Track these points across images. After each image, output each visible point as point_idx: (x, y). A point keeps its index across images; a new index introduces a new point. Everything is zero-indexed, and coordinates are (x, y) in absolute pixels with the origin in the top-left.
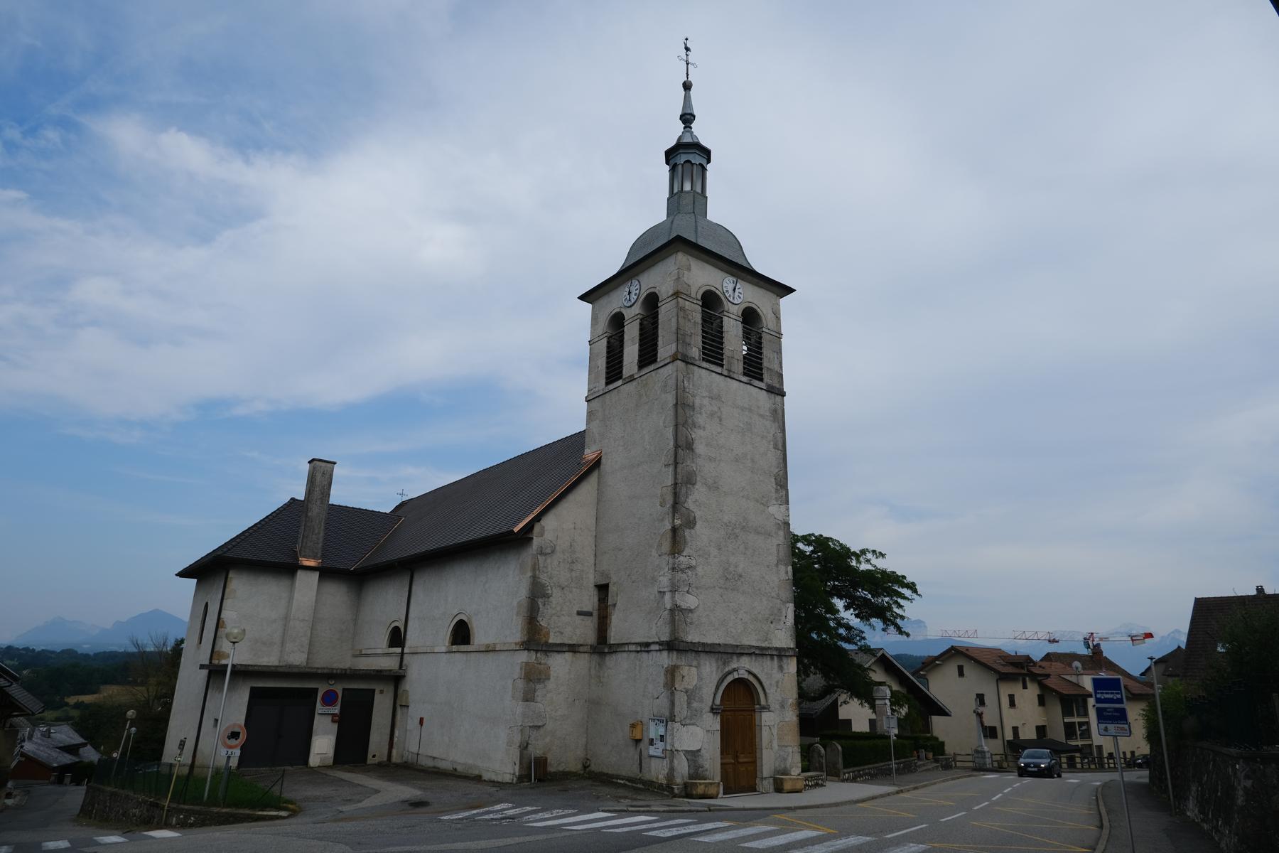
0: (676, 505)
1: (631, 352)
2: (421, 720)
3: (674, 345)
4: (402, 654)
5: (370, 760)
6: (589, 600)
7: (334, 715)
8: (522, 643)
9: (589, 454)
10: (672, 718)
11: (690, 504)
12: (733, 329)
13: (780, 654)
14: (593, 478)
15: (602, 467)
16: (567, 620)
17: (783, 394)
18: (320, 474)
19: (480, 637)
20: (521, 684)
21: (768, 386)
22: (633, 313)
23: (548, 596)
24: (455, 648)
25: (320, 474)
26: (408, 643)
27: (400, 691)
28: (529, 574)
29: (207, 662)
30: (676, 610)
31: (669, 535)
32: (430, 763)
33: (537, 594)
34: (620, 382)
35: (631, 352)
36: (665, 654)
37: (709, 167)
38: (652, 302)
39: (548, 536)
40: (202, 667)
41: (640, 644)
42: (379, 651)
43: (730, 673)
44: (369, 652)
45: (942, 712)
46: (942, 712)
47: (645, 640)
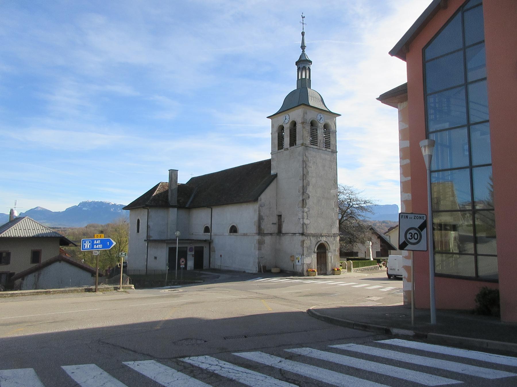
2: (221, 256)
5: (204, 268)
6: (275, 220)
9: (273, 172)
10: (303, 254)
12: (320, 133)
13: (334, 235)
14: (275, 181)
16: (269, 227)
17: (337, 152)
18: (173, 174)
20: (257, 245)
22: (287, 127)
23: (264, 219)
24: (232, 234)
25: (173, 174)
27: (211, 247)
30: (304, 224)
31: (302, 202)
32: (226, 268)
33: (260, 219)
38: (294, 124)
39: (263, 201)
40: (145, 241)
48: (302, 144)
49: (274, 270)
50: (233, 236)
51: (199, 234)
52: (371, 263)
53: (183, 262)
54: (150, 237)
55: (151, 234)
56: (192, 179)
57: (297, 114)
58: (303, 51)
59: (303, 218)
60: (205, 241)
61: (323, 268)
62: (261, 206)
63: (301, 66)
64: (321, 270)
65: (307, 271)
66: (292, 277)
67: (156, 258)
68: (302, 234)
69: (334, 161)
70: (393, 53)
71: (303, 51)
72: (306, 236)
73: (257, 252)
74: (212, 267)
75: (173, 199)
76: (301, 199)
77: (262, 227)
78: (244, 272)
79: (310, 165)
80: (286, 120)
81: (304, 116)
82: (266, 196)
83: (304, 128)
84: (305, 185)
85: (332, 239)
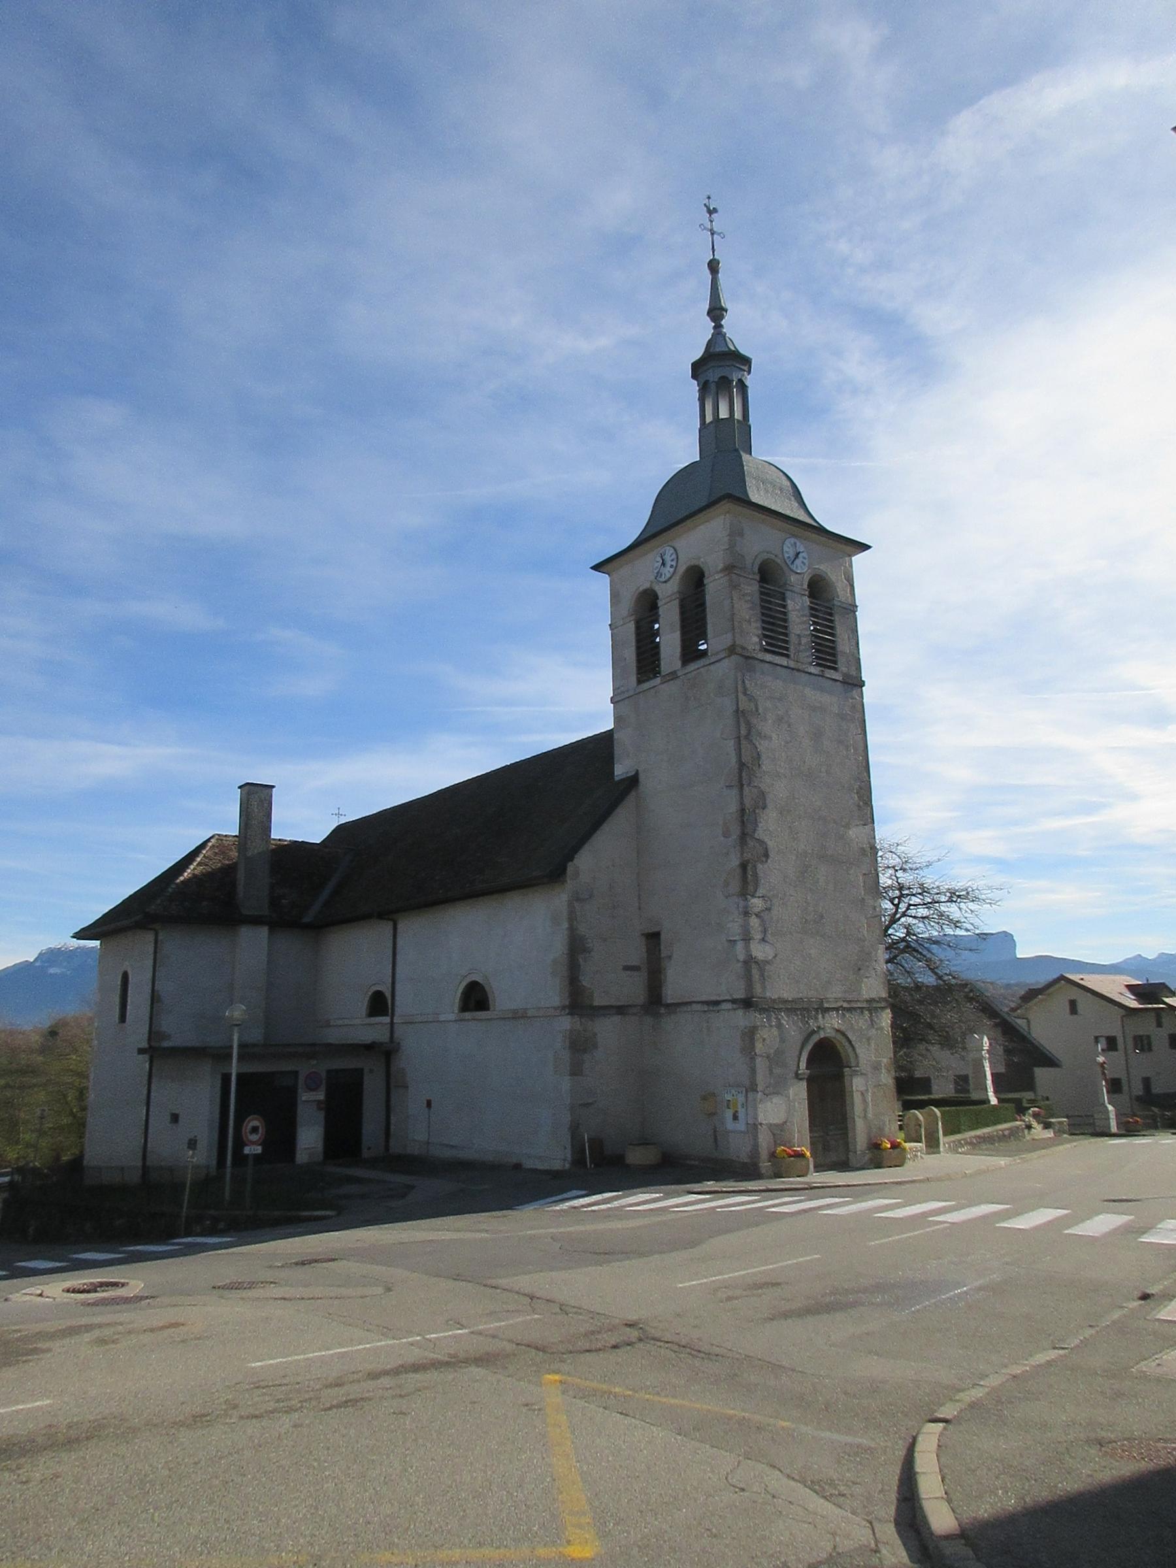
0: (744, 837)
1: (669, 641)
2: (429, 1104)
3: (729, 635)
4: (392, 1023)
5: (366, 1154)
6: (636, 953)
7: (319, 1102)
8: (564, 1008)
9: (620, 770)
10: (753, 1088)
11: (760, 833)
12: (797, 606)
13: (872, 1007)
15: (641, 788)
16: (612, 981)
17: (862, 684)
18: (256, 800)
19: (503, 998)
21: (845, 675)
22: (669, 592)
24: (467, 1015)
25: (256, 800)
26: (398, 1011)
28: (566, 925)
29: (145, 1045)
31: (739, 871)
32: (448, 1154)
33: (576, 948)
34: (658, 680)
35: (669, 641)
36: (740, 1012)
37: (749, 380)
38: (695, 578)
40: (141, 1051)
41: (707, 1003)
42: (358, 1021)
43: (813, 1032)
44: (340, 1022)
45: (1049, 1061)
46: (1049, 1061)
47: (714, 998)
48: (732, 650)
49: (636, 1157)
50: (476, 1023)
51: (350, 1022)
52: (994, 1116)
53: (255, 1130)
54: (164, 1036)
55: (167, 1024)
56: (340, 829)
57: (705, 542)
58: (718, 327)
59: (747, 939)
60: (370, 1047)
61: (835, 1142)
62: (577, 898)
63: (713, 375)
64: (826, 1148)
65: (773, 1155)
66: (710, 1185)
67: (175, 1118)
68: (747, 1003)
69: (857, 717)
70: (637, 775)
71: (718, 327)
72: (763, 1010)
73: (566, 1084)
74: (395, 1147)
75: (253, 893)
76: (735, 862)
77: (585, 982)
78: (517, 1167)
79: (767, 726)
80: (661, 574)
81: (732, 546)
82: (600, 859)
83: (734, 586)
84: (748, 803)
85: (860, 1022)
